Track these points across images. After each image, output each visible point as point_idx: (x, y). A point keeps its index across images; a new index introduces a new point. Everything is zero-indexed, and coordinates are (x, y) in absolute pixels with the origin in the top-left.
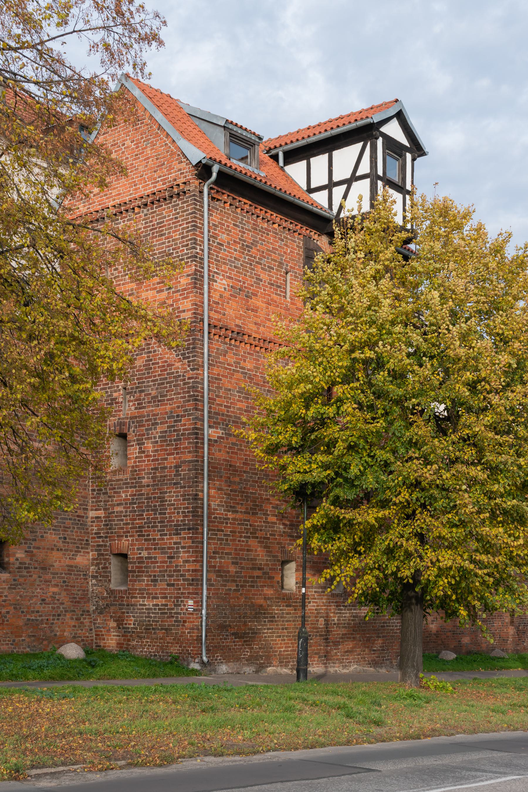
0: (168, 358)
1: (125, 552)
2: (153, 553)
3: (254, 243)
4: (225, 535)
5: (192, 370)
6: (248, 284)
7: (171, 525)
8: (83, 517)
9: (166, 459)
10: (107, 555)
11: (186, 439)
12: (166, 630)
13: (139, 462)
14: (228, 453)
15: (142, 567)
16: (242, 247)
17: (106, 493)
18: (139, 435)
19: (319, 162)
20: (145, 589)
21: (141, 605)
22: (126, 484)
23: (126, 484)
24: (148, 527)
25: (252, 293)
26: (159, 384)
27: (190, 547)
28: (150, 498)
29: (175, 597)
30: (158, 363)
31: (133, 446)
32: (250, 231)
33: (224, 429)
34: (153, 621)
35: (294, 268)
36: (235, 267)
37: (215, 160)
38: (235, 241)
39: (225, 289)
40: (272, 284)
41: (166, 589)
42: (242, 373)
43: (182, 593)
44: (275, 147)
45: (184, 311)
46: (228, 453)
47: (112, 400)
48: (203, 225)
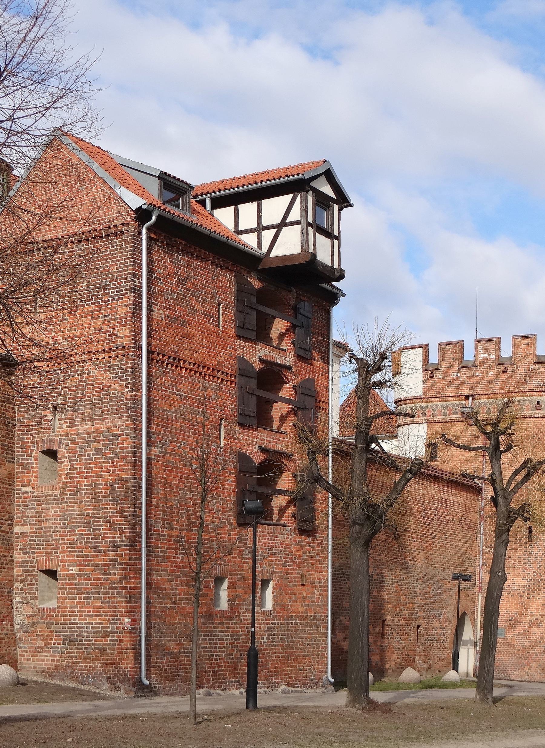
0: (105, 380)
1: (54, 569)
2: (86, 570)
3: (189, 278)
4: (161, 552)
5: (130, 391)
6: (183, 314)
7: (106, 542)
8: (8, 532)
9: (101, 476)
10: (33, 571)
11: (123, 457)
12: (100, 649)
13: (71, 478)
14: (165, 470)
15: (73, 584)
16: (178, 282)
17: (34, 509)
18: (71, 452)
19: (248, 210)
20: (76, 607)
21: (71, 623)
22: (55, 499)
23: (55, 499)
24: (81, 543)
25: (187, 322)
26: (93, 404)
27: (127, 564)
28: (83, 514)
29: (110, 616)
30: (93, 384)
31: (64, 462)
32: (186, 267)
33: (161, 448)
34: (85, 641)
35: (226, 300)
36: (171, 298)
37: (155, 206)
38: (170, 276)
39: (162, 318)
40: (205, 314)
41: (101, 607)
42: (178, 395)
43: (118, 611)
44: (202, 194)
45: (122, 337)
46: (165, 470)
47: (40, 417)
48: (142, 261)
